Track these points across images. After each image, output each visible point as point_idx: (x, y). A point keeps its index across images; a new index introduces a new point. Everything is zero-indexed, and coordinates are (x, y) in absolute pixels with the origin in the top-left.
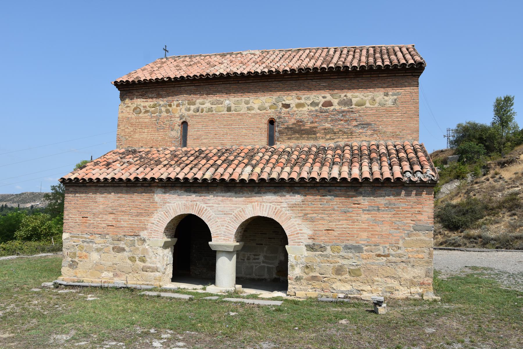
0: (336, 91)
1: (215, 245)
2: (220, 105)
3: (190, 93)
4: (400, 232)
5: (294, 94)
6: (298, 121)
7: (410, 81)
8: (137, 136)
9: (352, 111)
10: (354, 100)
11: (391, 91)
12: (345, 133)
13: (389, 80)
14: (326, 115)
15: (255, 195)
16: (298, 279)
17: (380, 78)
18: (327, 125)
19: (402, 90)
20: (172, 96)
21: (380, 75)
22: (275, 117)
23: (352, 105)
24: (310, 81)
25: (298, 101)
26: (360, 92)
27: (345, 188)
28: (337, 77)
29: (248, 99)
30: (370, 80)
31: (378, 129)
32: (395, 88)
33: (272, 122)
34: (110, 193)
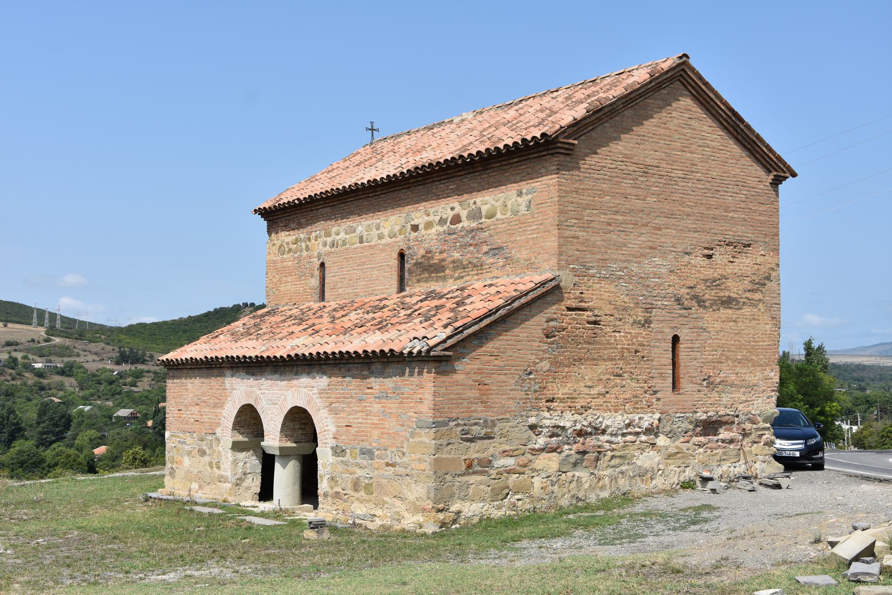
0: (465, 196)
1: (266, 447)
2: (353, 235)
3: (328, 218)
4: (405, 430)
5: (422, 206)
6: (427, 252)
7: (548, 165)
8: (282, 288)
9: (482, 229)
10: (484, 209)
11: (525, 186)
12: (475, 266)
13: (523, 167)
14: (454, 239)
15: (294, 377)
16: (326, 495)
17: (513, 165)
18: (457, 255)
19: (538, 183)
20: (311, 224)
21: (511, 161)
22: (404, 247)
23: (481, 218)
24: (438, 183)
25: (427, 218)
26: (490, 194)
27: (360, 365)
28: (463, 173)
29: (378, 221)
30: (502, 171)
31: (510, 255)
32: (530, 181)
33: (402, 256)
34: (196, 377)
